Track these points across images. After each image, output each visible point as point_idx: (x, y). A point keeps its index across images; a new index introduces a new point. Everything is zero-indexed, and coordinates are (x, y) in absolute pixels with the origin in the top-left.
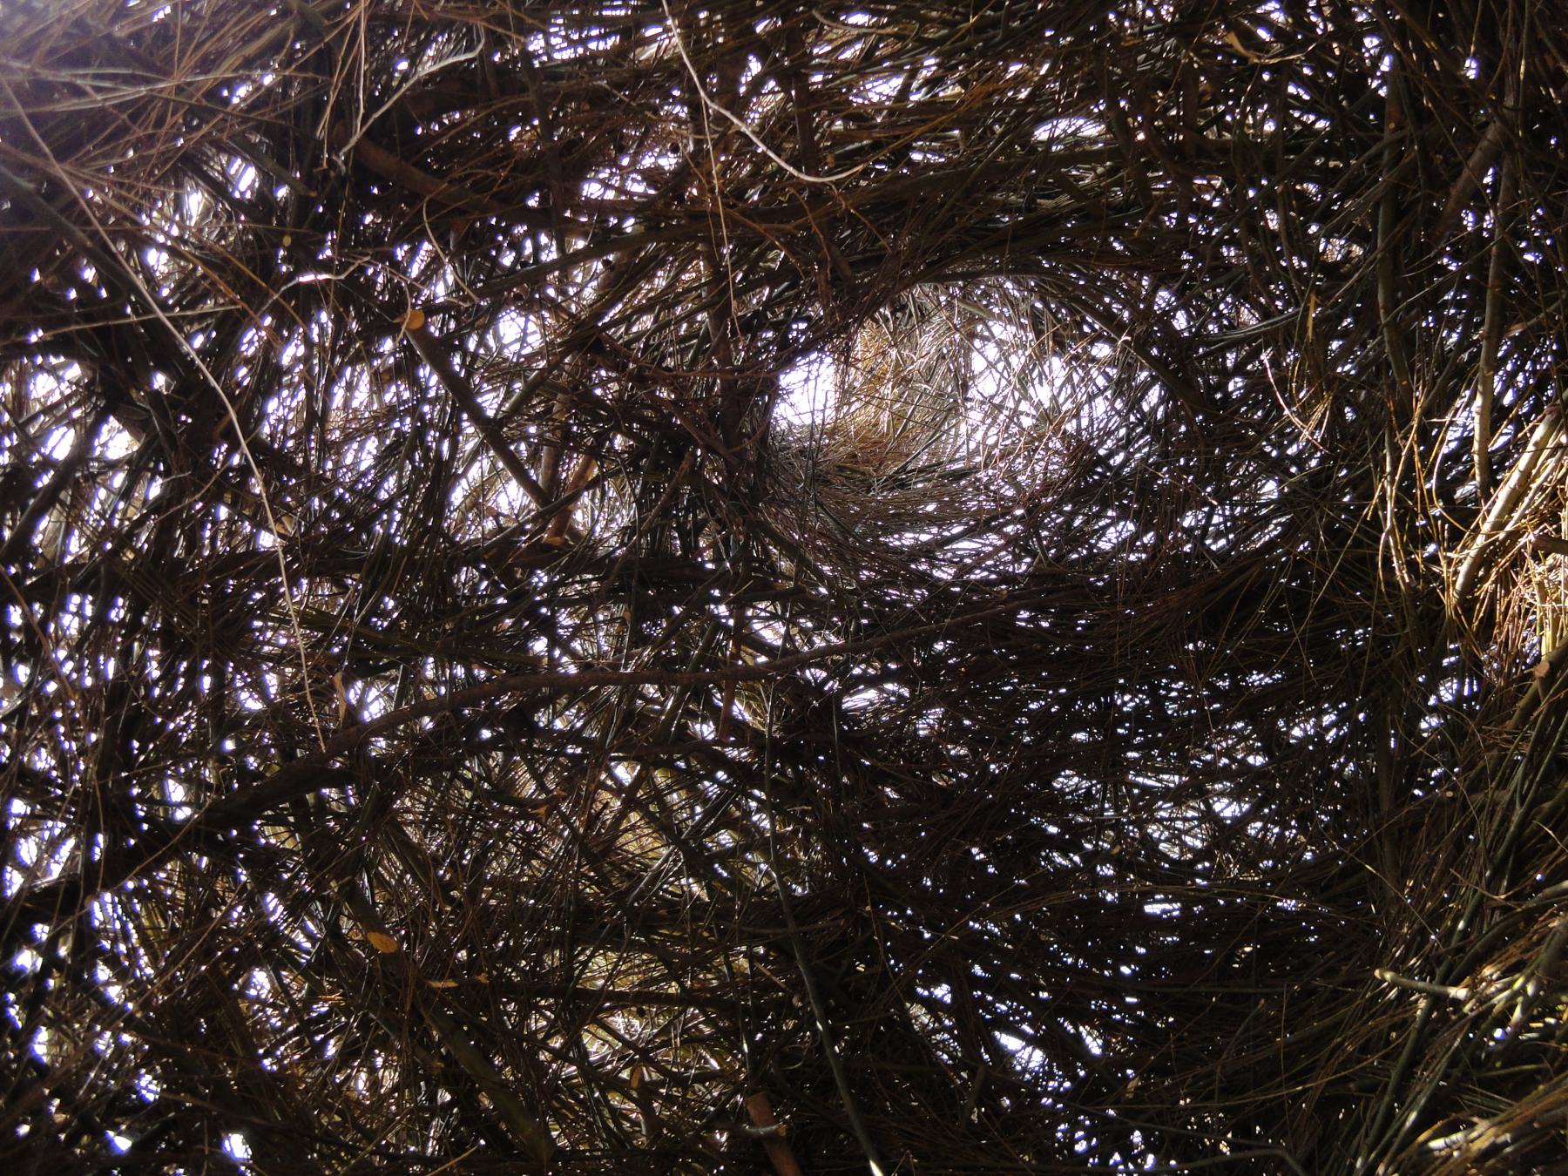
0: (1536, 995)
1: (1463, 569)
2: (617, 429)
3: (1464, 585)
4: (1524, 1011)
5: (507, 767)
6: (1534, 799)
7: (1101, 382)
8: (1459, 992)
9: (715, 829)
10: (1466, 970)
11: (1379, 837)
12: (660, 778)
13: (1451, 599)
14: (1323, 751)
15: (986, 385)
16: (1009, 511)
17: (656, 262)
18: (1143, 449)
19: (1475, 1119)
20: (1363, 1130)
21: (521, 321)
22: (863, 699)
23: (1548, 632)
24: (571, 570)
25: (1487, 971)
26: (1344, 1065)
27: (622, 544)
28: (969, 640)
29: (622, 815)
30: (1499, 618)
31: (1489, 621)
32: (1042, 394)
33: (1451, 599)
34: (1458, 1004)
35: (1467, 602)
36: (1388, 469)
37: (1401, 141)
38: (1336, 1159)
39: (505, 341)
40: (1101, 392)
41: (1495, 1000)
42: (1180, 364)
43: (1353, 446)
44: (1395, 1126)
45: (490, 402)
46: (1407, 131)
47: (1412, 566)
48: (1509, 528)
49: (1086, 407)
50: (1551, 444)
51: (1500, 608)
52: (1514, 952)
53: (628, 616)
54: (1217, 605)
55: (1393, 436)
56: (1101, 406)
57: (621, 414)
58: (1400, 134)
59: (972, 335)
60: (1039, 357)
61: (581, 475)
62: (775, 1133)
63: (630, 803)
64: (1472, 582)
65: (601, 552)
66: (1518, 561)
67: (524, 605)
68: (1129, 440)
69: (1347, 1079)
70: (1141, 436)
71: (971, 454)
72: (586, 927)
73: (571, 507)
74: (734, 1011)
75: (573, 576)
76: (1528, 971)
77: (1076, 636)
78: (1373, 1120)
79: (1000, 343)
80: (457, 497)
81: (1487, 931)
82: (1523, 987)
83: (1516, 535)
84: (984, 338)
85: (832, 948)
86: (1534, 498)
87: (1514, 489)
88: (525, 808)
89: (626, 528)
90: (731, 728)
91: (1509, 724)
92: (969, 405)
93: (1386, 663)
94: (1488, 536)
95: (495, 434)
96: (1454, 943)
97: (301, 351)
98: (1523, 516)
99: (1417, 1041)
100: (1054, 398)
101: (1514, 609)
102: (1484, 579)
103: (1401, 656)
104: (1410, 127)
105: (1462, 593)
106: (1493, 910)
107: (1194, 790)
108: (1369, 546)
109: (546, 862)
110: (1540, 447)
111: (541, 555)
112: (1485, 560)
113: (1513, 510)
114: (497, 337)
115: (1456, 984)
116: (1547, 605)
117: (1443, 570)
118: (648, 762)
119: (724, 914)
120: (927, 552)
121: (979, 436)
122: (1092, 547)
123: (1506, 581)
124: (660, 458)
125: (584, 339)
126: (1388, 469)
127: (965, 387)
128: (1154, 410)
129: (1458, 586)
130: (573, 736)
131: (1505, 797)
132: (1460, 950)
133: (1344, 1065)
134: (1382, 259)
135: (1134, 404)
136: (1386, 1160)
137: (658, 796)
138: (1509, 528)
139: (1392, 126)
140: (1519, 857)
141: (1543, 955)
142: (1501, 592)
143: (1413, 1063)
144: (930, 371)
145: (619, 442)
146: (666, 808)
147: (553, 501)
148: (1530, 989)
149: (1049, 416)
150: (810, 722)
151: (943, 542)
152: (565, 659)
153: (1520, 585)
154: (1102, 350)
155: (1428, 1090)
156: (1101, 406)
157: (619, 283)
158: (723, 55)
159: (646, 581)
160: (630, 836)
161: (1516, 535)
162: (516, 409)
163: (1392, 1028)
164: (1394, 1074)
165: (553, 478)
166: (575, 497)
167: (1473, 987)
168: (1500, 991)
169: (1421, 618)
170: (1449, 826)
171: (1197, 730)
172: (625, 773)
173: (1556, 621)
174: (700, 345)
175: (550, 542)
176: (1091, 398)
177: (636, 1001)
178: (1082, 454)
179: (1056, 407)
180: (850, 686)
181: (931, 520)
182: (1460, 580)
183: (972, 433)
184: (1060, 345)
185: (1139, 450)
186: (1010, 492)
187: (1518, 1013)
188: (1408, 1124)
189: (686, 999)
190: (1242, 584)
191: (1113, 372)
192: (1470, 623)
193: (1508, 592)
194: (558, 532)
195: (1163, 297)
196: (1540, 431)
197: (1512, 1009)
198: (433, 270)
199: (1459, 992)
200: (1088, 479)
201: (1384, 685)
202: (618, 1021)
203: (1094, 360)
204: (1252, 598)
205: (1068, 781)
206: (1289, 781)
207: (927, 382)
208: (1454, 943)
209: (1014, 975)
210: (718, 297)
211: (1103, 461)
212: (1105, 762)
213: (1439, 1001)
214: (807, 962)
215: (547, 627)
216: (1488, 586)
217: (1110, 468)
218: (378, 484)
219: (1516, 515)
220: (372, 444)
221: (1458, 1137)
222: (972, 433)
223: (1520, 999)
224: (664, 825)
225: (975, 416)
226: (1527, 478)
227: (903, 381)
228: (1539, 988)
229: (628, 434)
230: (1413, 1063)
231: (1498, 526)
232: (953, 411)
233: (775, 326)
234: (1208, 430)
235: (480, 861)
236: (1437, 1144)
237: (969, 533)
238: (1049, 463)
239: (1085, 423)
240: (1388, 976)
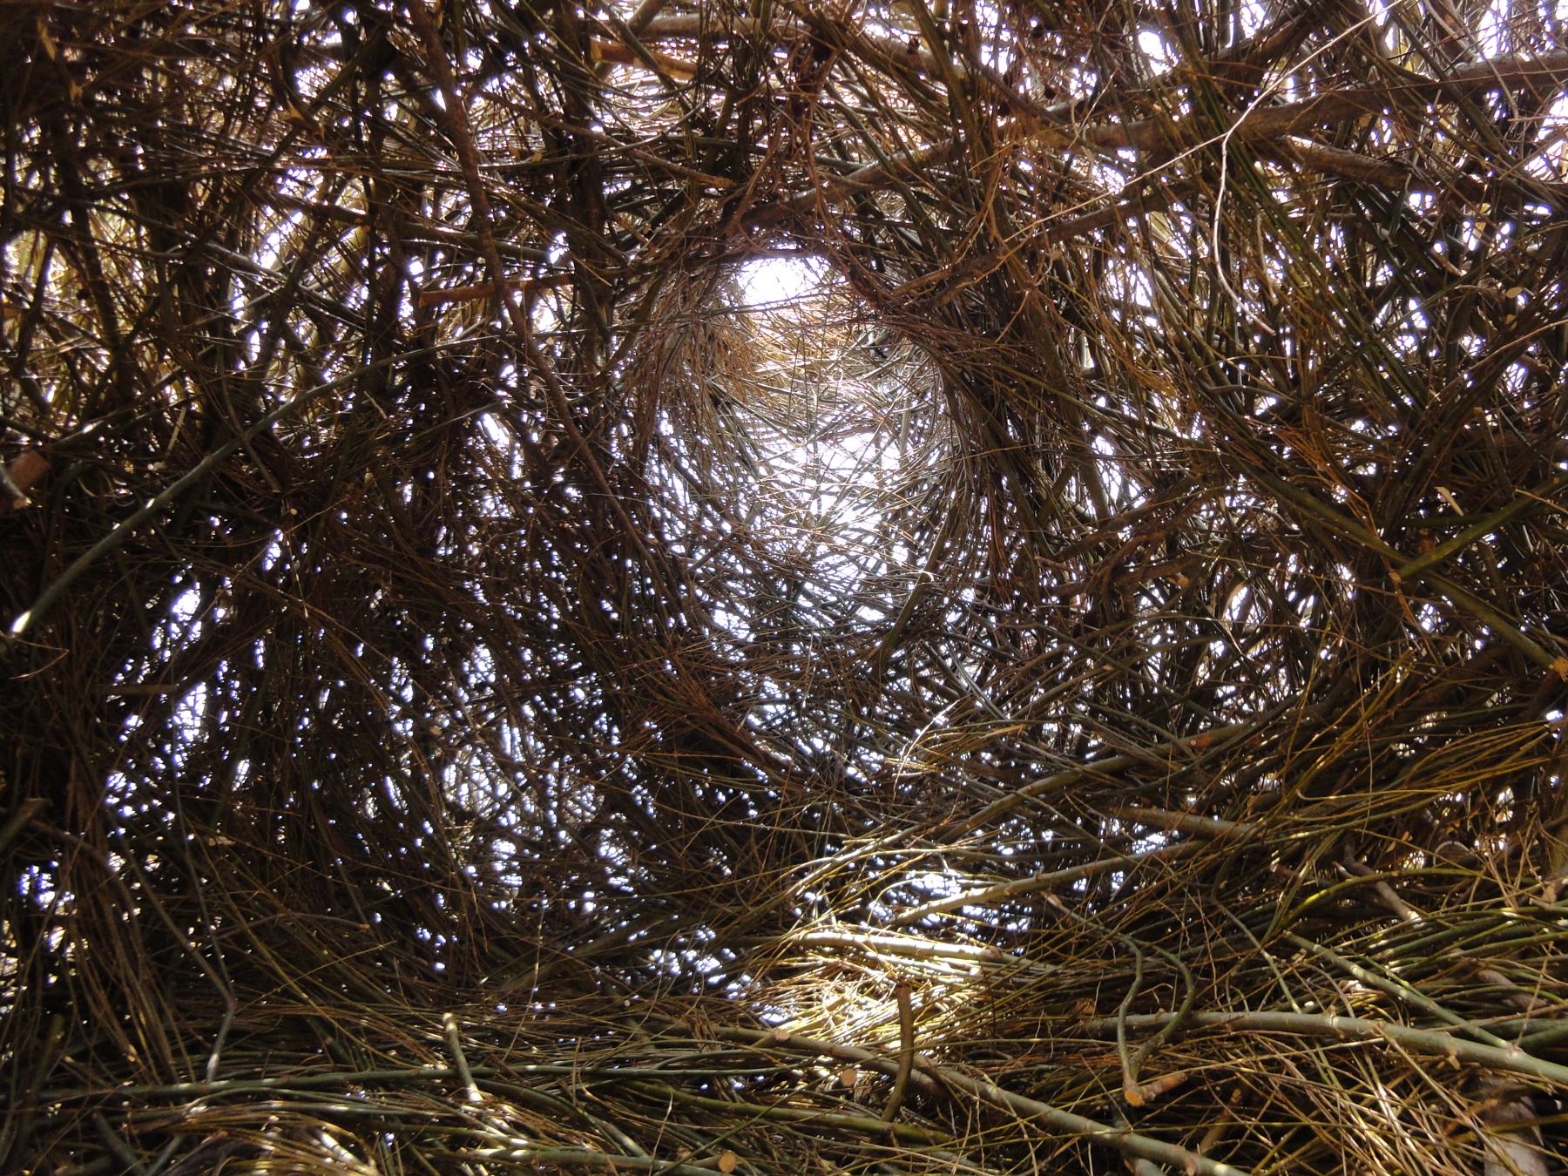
0: (514, 1160)
1: (828, 934)
2: (733, 95)
4: (493, 1156)
6: (670, 1076)
7: (871, 564)
8: (475, 1094)
10: (499, 1092)
11: (545, 954)
12: (351, 237)
13: (796, 934)
14: (596, 873)
16: (724, 516)
17: (923, 97)
19: (372, 1162)
20: (296, 1068)
22: (495, 430)
23: (805, 1022)
25: (507, 1108)
26: (344, 1023)
27: (608, 131)
28: (598, 518)
30: (798, 978)
31: (790, 972)
32: (848, 516)
33: (796, 934)
35: (798, 949)
36: (887, 840)
37: (1182, 754)
38: (255, 1057)
41: (489, 1128)
42: (916, 624)
43: (884, 801)
44: (321, 1095)
46: (1193, 757)
48: (882, 958)
49: (843, 558)
50: (966, 963)
51: (806, 976)
52: (536, 1122)
54: (705, 733)
55: (916, 833)
56: (849, 571)
57: (746, 94)
58: (1188, 751)
60: (879, 499)
61: (674, 66)
62: (11, 497)
66: (852, 975)
67: (518, 30)
70: (833, 617)
71: (765, 463)
72: (157, 200)
73: (637, 61)
74: (119, 399)
75: (561, 80)
76: (533, 1143)
77: (618, 616)
78: (311, 1074)
79: (877, 459)
81: (541, 1091)
82: (517, 1147)
83: (874, 964)
85: (234, 474)
86: (912, 967)
87: (914, 948)
88: (284, 90)
89: (630, 132)
91: (715, 1027)
92: (810, 447)
93: (713, 902)
94: (867, 943)
96: (512, 1068)
98: (895, 964)
99: (410, 1078)
100: (845, 527)
101: (810, 988)
102: (821, 953)
103: (725, 913)
104: (1197, 759)
106: (558, 1087)
108: (811, 848)
109: (224, 131)
110: (961, 955)
112: (840, 948)
113: (897, 954)
115: (481, 1087)
116: (827, 1014)
117: (817, 920)
122: (714, 606)
123: (830, 972)
124: (719, 151)
126: (887, 840)
127: (824, 440)
128: (862, 621)
129: (810, 936)
131: (652, 1051)
132: (508, 1074)
133: (344, 1023)
134: (1076, 773)
135: (860, 600)
136: (289, 1104)
138: (882, 958)
139: (1193, 743)
140: (613, 1088)
141: (556, 1150)
142: (819, 971)
143: (384, 1083)
144: (831, 400)
145: (717, 100)
148: (518, 1153)
150: (456, 388)
153: (833, 984)
154: (900, 554)
158: (1163, 124)
161: (874, 964)
163: (399, 1049)
164: (367, 1073)
166: (649, 64)
168: (501, 1129)
169: (768, 915)
170: (596, 1015)
172: (351, 197)
173: (819, 1024)
174: (836, 164)
176: (854, 560)
177: (93, 286)
178: (797, 569)
180: (509, 418)
181: (694, 446)
183: (784, 457)
185: (820, 619)
186: (743, 511)
187: (488, 1152)
188: (333, 1107)
189: (113, 340)
190: (732, 754)
191: (883, 571)
192: (782, 958)
193: (821, 977)
195: (969, 595)
197: (487, 1145)
199: (475, 1094)
201: (674, 901)
202: (58, 267)
203: (889, 550)
206: (558, 862)
207: (819, 399)
208: (512, 1068)
209: (20, 624)
210: (893, 176)
214: (213, 466)
215: (495, 65)
216: (821, 959)
219: (894, 958)
221: (347, 1156)
222: (784, 457)
223: (501, 1148)
224: (303, 256)
225: (801, 456)
226: (928, 955)
227: (813, 373)
229: (728, 109)
230: (384, 1083)
231: (880, 948)
234: (850, 680)
235: (198, 48)
236: (329, 1140)
238: (782, 542)
239: (830, 560)
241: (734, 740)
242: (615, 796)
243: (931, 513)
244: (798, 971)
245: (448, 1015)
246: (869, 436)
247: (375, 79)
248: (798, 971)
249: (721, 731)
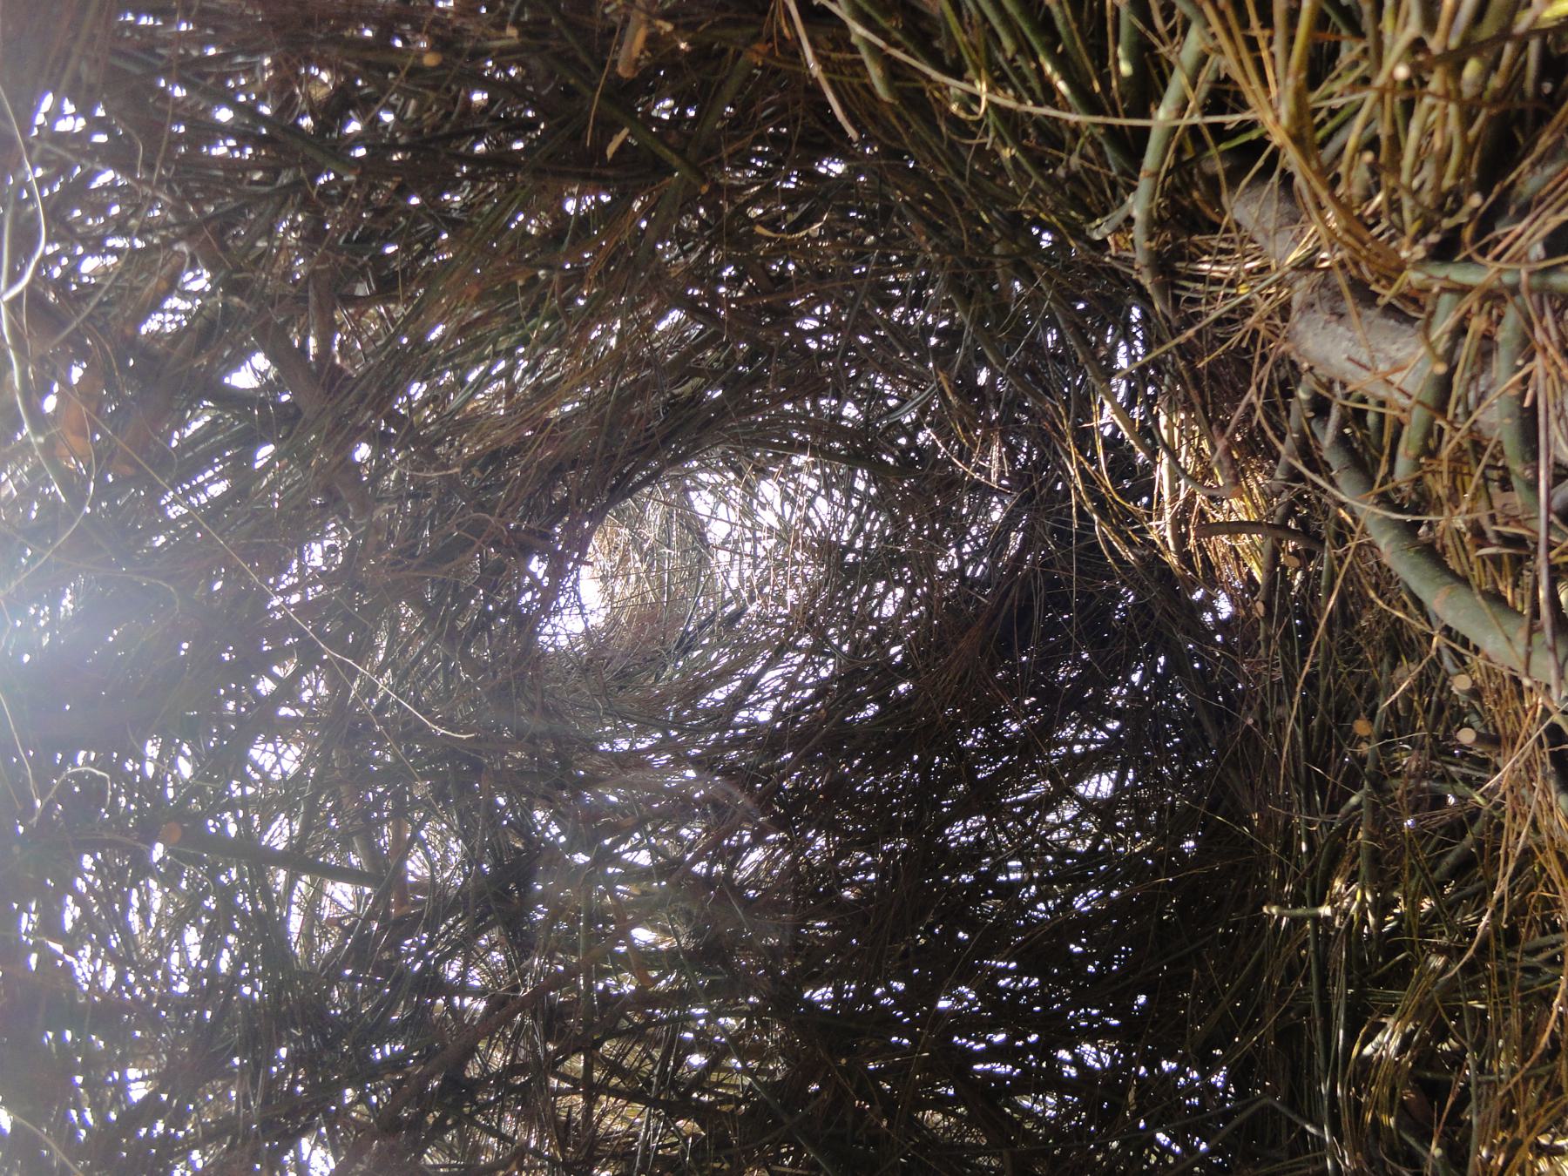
3: (1176, 546)
5: (463, 1139)
8: (1325, 910)
9: (679, 1062)
13: (1172, 559)
15: (717, 532)
18: (876, 524)
21: (270, 747)
24: (431, 927)
29: (588, 1112)
32: (768, 518)
33: (1172, 559)
34: (1328, 921)
39: (267, 768)
40: (817, 493)
42: (862, 448)
45: (279, 834)
47: (1130, 543)
48: (1183, 496)
52: (1344, 865)
53: (503, 940)
59: (687, 490)
60: (750, 490)
63: (592, 1091)
64: (1181, 539)
65: (452, 893)
68: (860, 523)
69: (1288, 1010)
77: (898, 741)
80: (295, 923)
84: (695, 489)
90: (644, 960)
95: (297, 859)
97: (78, 912)
99: (1318, 958)
100: (780, 518)
102: (1187, 535)
105: (1178, 551)
107: (1064, 791)
111: (402, 927)
112: (1179, 521)
114: (257, 768)
115: (1321, 904)
118: (589, 1048)
119: (722, 1144)
120: (736, 702)
121: (734, 574)
125: (340, 730)
130: (512, 1069)
135: (849, 491)
137: (614, 1068)
138: (1183, 496)
146: (624, 1074)
147: (383, 874)
149: (784, 534)
151: (751, 684)
152: (467, 1001)
154: (799, 460)
155: (1343, 1001)
156: (821, 503)
157: (339, 678)
159: (500, 894)
160: (607, 1120)
162: (306, 828)
165: (372, 852)
167: (1332, 903)
169: (1159, 580)
171: (1040, 736)
175: (399, 909)
176: (811, 503)
179: (786, 527)
182: (1171, 544)
184: (762, 472)
194: (402, 901)
196: (1163, 420)
198: (167, 760)
199: (1325, 910)
200: (843, 570)
203: (798, 469)
204: (1025, 611)
205: (958, 833)
211: (850, 547)
212: (985, 799)
213: (1317, 919)
217: (858, 552)
218: (214, 965)
220: (192, 936)
228: (1373, 894)
231: (1174, 499)
232: (703, 561)
233: (504, 612)
234: (922, 491)
236: (1368, 1050)
237: (769, 665)
240: (1274, 910)
241: (1001, 604)
242: (1061, 704)
243: (753, 445)
244: (1205, 559)
245: (1265, 910)
246: (693, 495)
247: (475, 1086)
248: (1205, 559)
249: (995, 617)
